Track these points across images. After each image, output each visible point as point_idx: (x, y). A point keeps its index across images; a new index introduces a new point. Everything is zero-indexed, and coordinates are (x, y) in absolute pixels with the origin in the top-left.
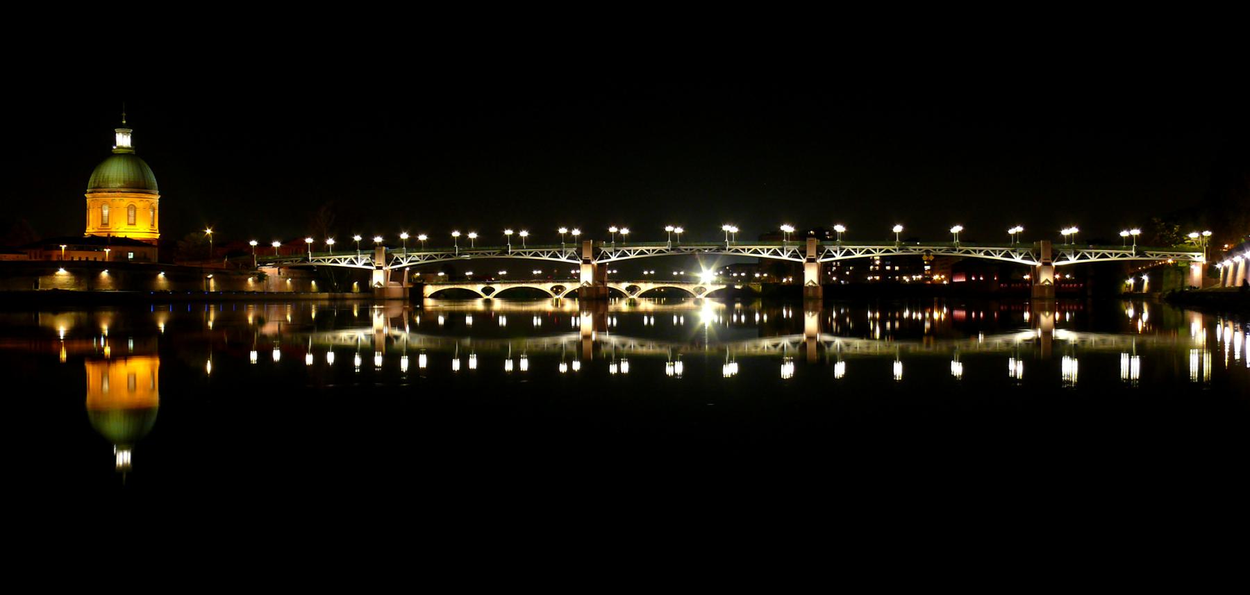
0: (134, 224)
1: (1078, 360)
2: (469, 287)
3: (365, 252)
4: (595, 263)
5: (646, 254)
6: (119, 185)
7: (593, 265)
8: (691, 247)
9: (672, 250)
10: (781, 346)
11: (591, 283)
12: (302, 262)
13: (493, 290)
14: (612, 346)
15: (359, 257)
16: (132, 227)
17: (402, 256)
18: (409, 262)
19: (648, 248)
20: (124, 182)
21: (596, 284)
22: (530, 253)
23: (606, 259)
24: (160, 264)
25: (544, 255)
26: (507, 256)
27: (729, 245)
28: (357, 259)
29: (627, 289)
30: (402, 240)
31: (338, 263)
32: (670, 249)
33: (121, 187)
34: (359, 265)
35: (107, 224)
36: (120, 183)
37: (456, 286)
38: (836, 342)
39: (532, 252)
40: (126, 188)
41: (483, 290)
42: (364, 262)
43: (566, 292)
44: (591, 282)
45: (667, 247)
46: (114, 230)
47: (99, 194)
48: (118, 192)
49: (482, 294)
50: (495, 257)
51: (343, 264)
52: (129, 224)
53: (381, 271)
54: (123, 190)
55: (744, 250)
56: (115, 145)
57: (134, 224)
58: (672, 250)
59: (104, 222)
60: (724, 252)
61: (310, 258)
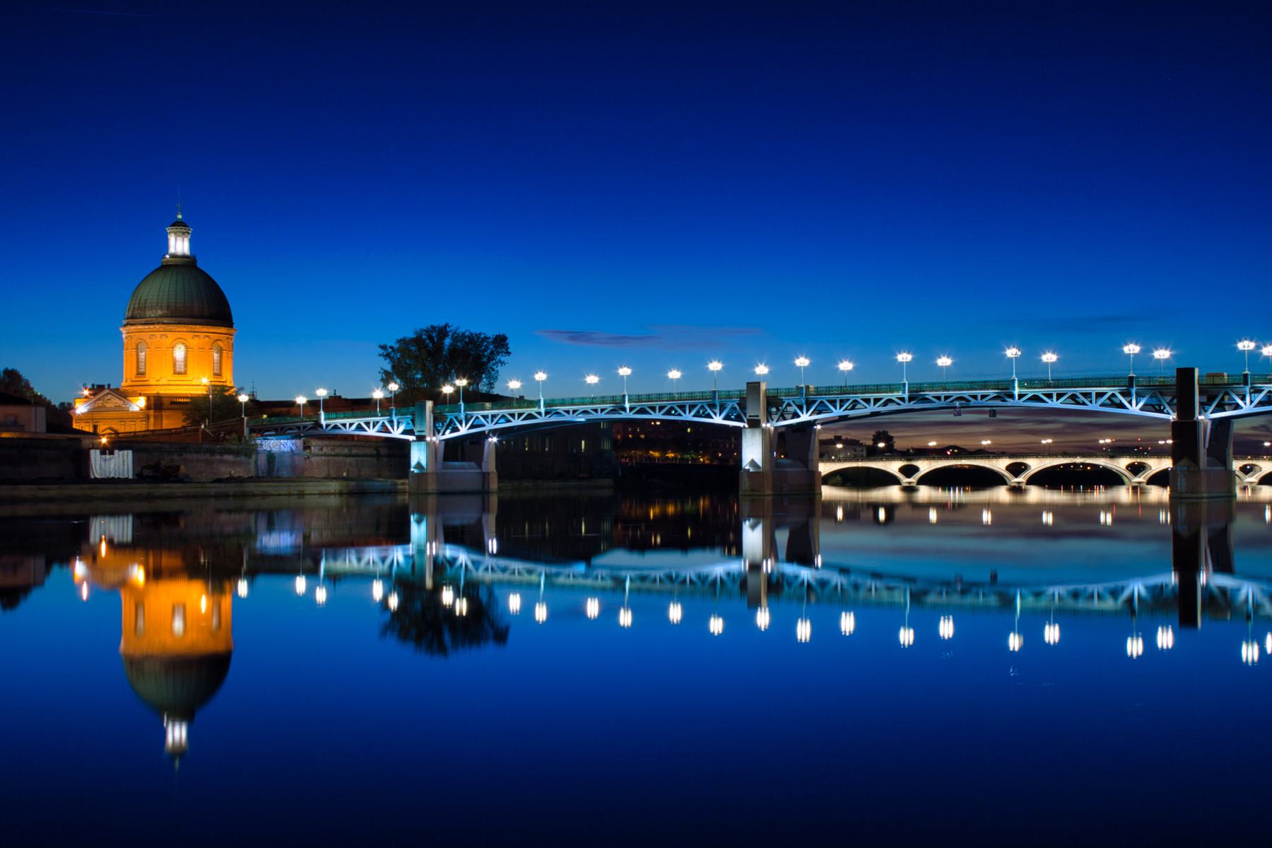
0: (185, 373)
1: (682, 605)
2: (1102, 462)
3: (404, 410)
4: (769, 426)
5: (535, 418)
6: (160, 312)
7: (764, 432)
8: (946, 393)
9: (911, 399)
10: (1126, 594)
11: (760, 463)
12: (613, 411)
13: (916, 469)
14: (803, 582)
15: (395, 419)
16: (181, 377)
17: (798, 402)
18: (470, 428)
19: (974, 392)
20: (168, 307)
21: (778, 465)
22: (877, 400)
23: (793, 418)
24: (50, 436)
25: (655, 412)
26: (623, 415)
27: (1020, 387)
28: (391, 422)
29: (1009, 468)
30: (446, 395)
31: (712, 418)
32: (906, 396)
33: (161, 316)
34: (397, 433)
35: (143, 374)
36: (161, 309)
37: (860, 464)
38: (486, 563)
39: (523, 414)
40: (172, 317)
41: (902, 470)
42: (402, 428)
43: (1149, 473)
44: (759, 462)
45: (900, 394)
46: (154, 383)
47: (133, 328)
48: (158, 323)
49: (1007, 474)
50: (603, 416)
51: (372, 432)
52: (175, 373)
53: (423, 445)
54: (165, 320)
55: (1050, 396)
56: (167, 253)
57: (185, 373)
58: (911, 399)
59: (178, 370)
60: (1010, 402)
61: (1017, 392)
